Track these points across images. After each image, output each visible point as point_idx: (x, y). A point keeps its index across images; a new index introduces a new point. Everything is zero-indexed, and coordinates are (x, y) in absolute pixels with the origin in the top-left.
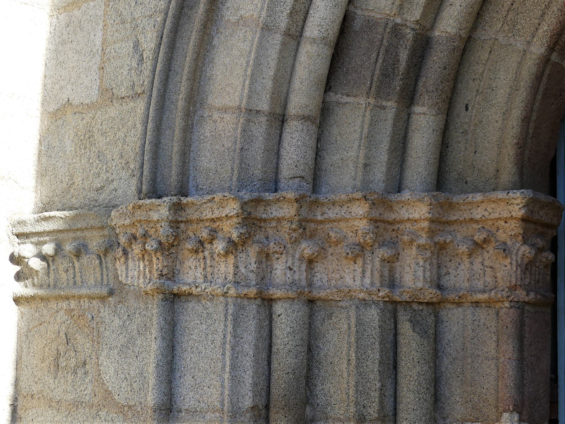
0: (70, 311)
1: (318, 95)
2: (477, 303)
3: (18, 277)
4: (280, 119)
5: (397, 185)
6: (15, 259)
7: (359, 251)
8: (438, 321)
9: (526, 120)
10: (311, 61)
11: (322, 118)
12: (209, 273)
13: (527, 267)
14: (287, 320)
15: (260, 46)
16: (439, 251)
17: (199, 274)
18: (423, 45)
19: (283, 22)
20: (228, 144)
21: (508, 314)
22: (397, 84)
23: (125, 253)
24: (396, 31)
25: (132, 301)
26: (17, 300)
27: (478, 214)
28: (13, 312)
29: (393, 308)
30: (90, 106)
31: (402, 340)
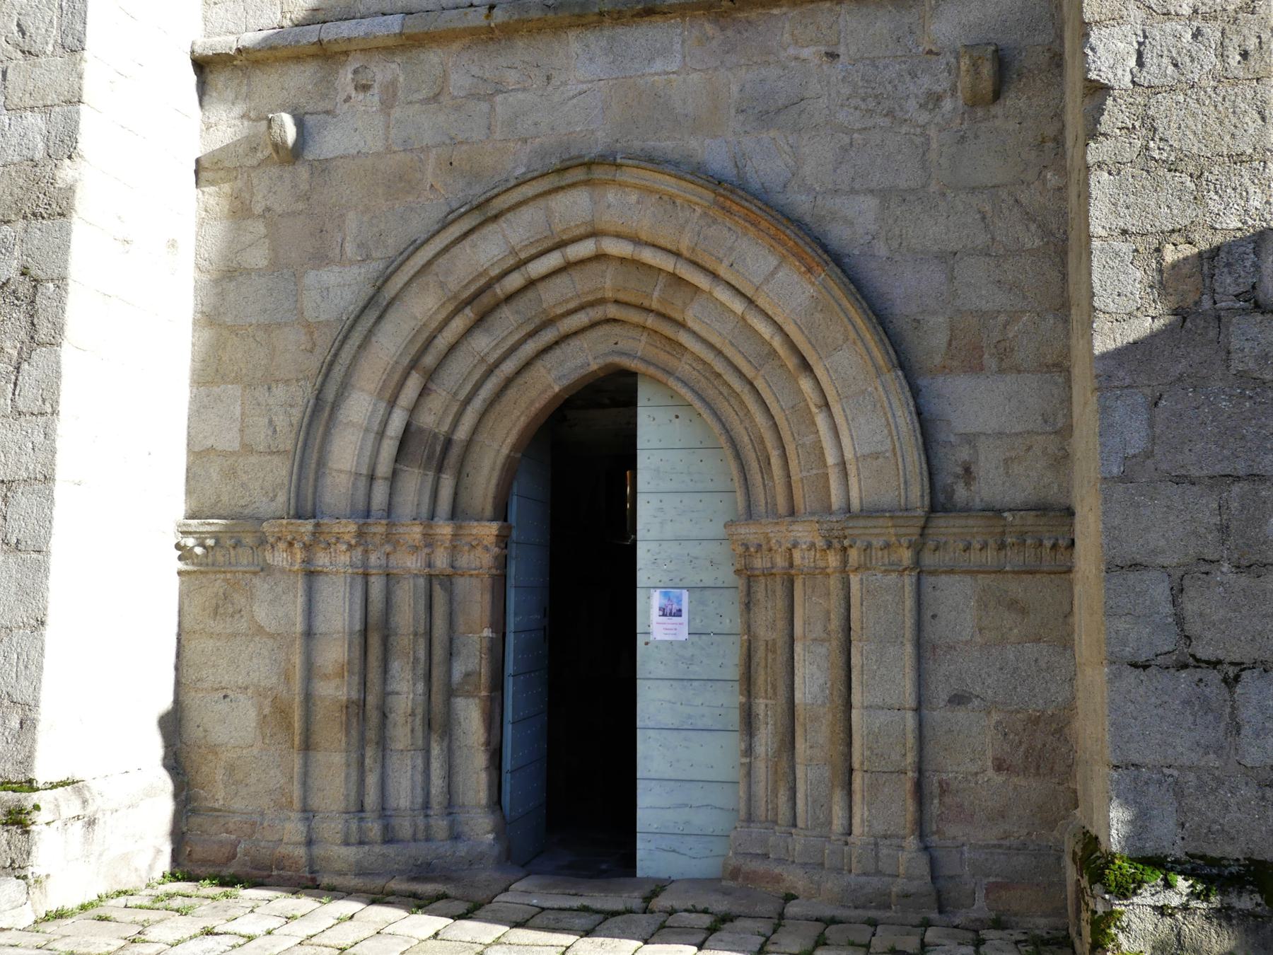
0: (226, 581)
1: (391, 465)
2: (471, 575)
3: (180, 558)
4: (372, 478)
5: (432, 516)
6: (178, 546)
7: (415, 549)
8: (451, 584)
9: (498, 485)
10: (389, 448)
11: (394, 476)
12: (337, 561)
13: (496, 558)
14: (377, 585)
15: (363, 439)
16: (454, 549)
17: (327, 560)
18: (448, 442)
19: (376, 427)
20: (343, 490)
21: (487, 581)
22: (434, 463)
23: (273, 547)
24: (435, 436)
25: (278, 575)
26: (180, 573)
27: (474, 531)
28: (176, 580)
29: (430, 578)
30: (233, 453)
31: (435, 594)
